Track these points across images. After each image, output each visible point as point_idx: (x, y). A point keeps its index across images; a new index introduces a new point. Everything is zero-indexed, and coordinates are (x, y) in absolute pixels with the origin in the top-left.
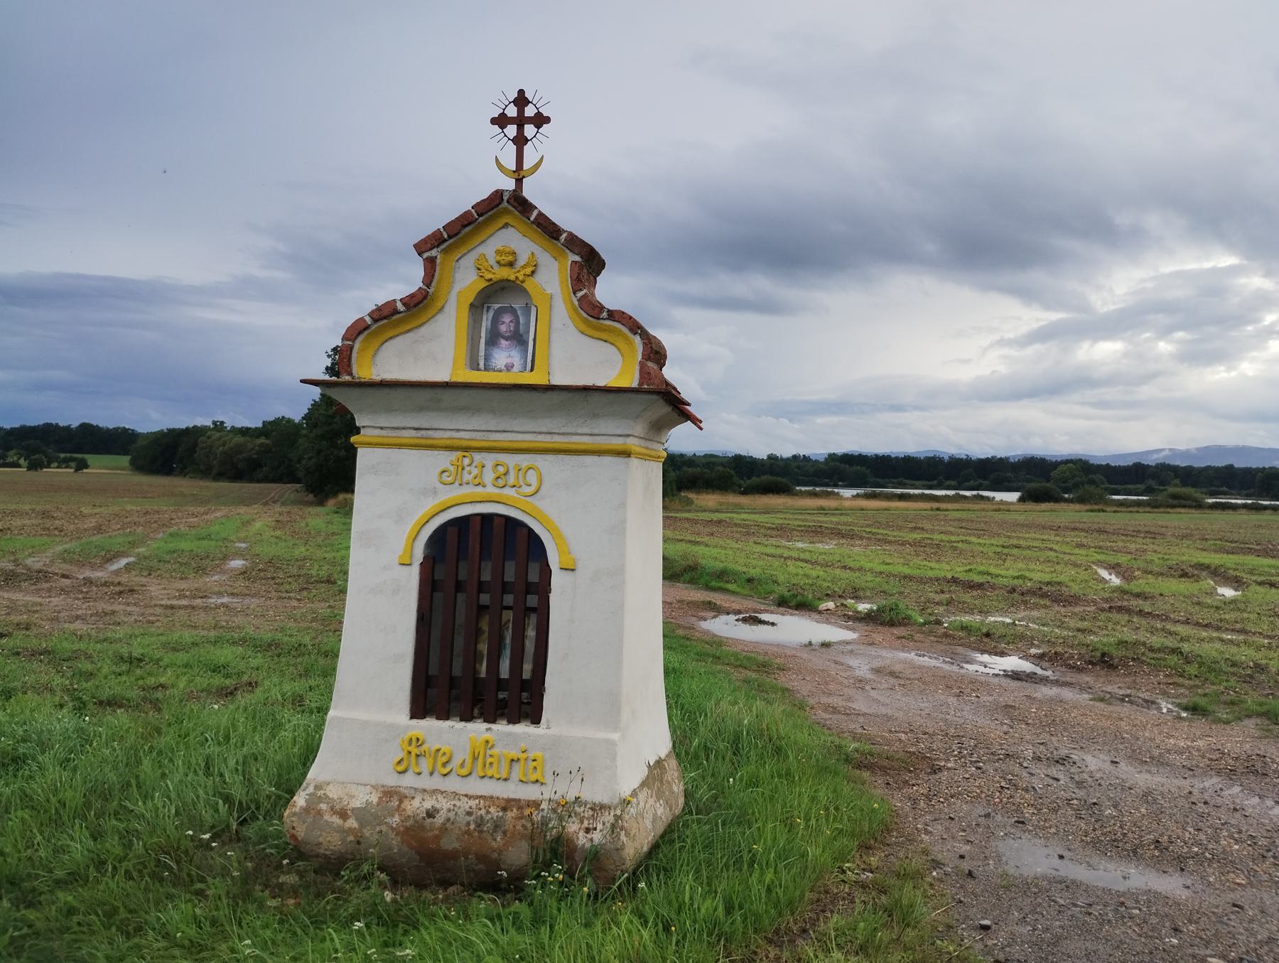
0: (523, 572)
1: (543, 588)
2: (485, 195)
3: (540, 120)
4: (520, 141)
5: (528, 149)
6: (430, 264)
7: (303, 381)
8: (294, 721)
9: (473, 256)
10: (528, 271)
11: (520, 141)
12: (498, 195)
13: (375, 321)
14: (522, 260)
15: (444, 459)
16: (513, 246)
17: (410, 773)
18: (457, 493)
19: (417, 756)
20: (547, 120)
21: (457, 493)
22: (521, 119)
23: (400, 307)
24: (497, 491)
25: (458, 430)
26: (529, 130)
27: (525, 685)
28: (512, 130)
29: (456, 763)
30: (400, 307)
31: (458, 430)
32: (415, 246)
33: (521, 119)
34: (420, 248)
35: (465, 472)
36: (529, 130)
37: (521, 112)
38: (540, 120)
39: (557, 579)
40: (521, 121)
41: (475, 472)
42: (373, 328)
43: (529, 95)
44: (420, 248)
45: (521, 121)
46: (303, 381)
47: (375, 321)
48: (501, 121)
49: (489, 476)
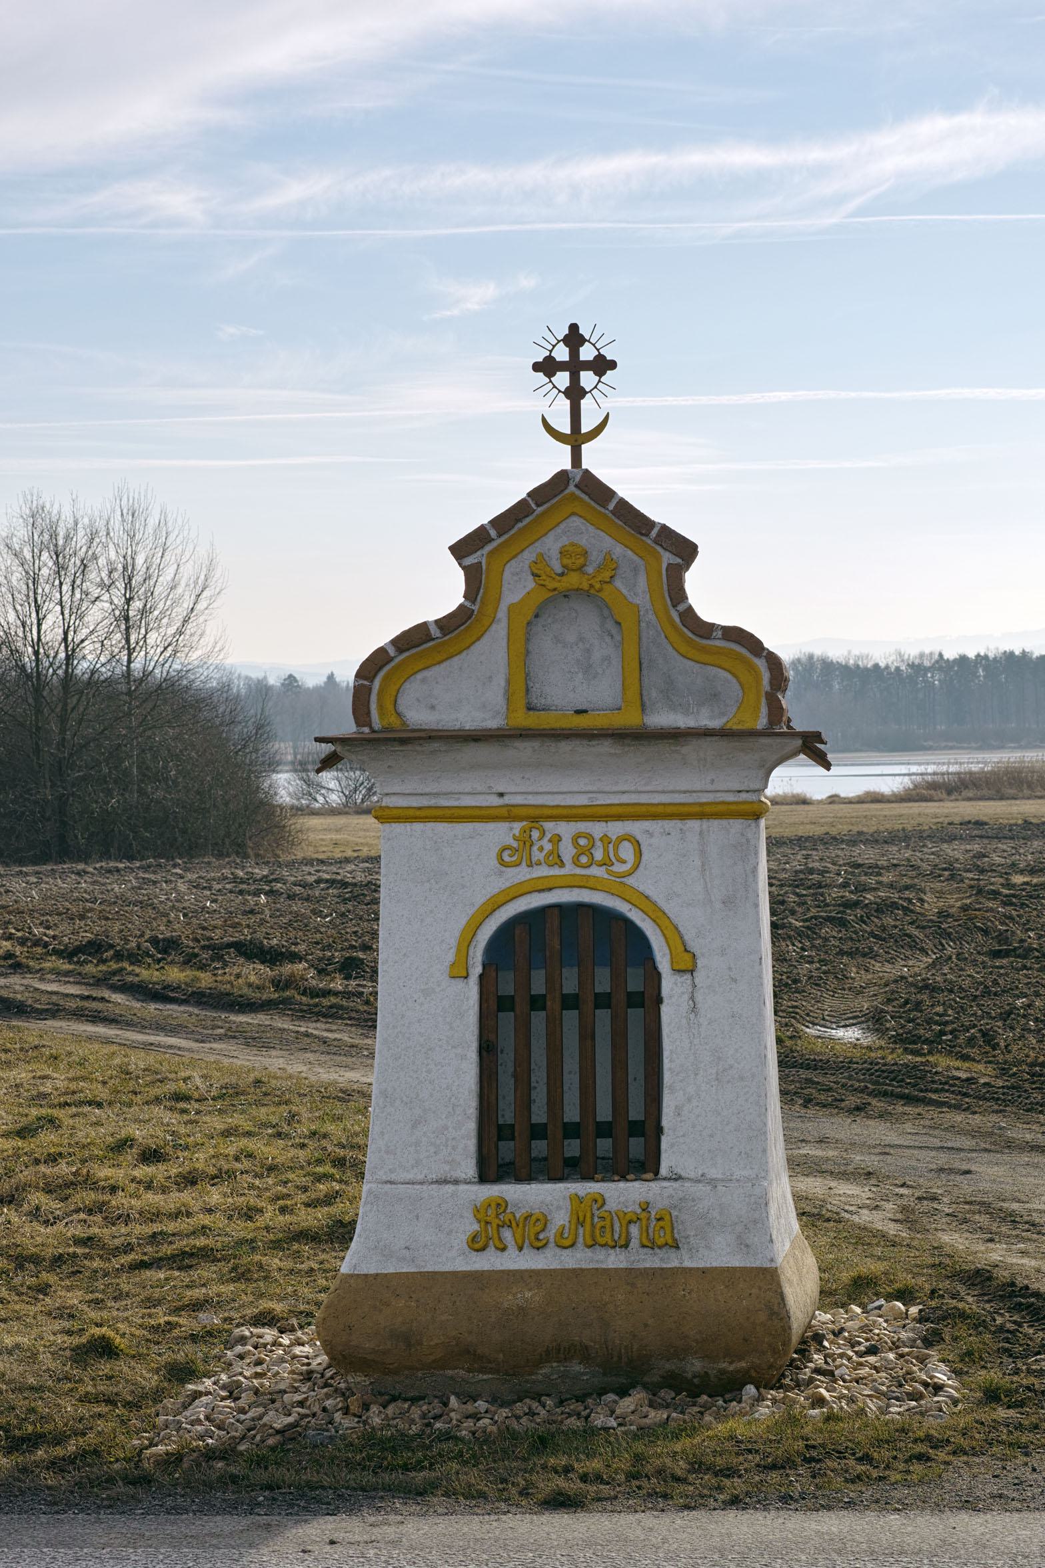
0: (618, 978)
1: (649, 1000)
2: (545, 477)
3: (602, 365)
4: (575, 393)
5: (586, 403)
6: (473, 578)
7: (317, 740)
8: (507, 986)
9: (528, 556)
10: (606, 575)
11: (575, 393)
12: (561, 478)
13: (400, 651)
14: (595, 558)
15: (502, 833)
16: (583, 541)
17: (491, 1249)
18: (522, 874)
19: (498, 1226)
20: (612, 365)
21: (522, 874)
22: (575, 363)
23: (435, 631)
24: (578, 871)
25: (437, 795)
26: (587, 379)
27: (636, 1129)
28: (563, 379)
29: (551, 1233)
30: (435, 631)
31: (437, 795)
32: (450, 548)
33: (575, 363)
34: (460, 550)
35: (535, 848)
36: (587, 379)
37: (574, 353)
38: (602, 365)
39: (670, 985)
40: (575, 366)
41: (548, 847)
42: (397, 660)
43: (584, 331)
44: (460, 550)
45: (575, 366)
46: (317, 740)
47: (400, 651)
48: (547, 367)
49: (567, 851)
